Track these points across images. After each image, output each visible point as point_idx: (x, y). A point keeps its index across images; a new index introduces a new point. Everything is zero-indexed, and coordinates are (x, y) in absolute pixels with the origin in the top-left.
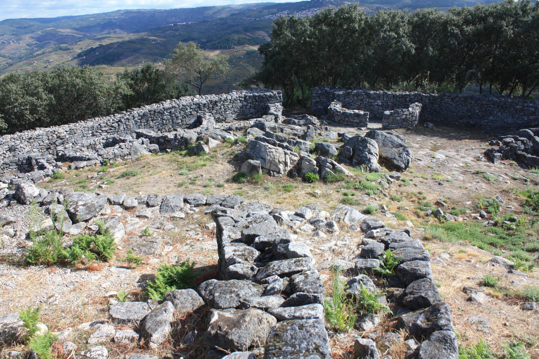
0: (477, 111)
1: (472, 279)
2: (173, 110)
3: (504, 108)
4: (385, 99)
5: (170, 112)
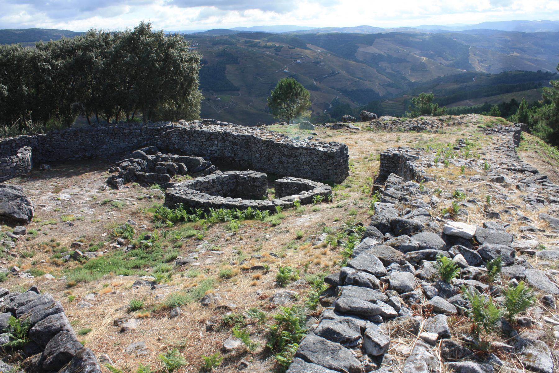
0: (90, 142)
1: (120, 309)
3: (114, 134)
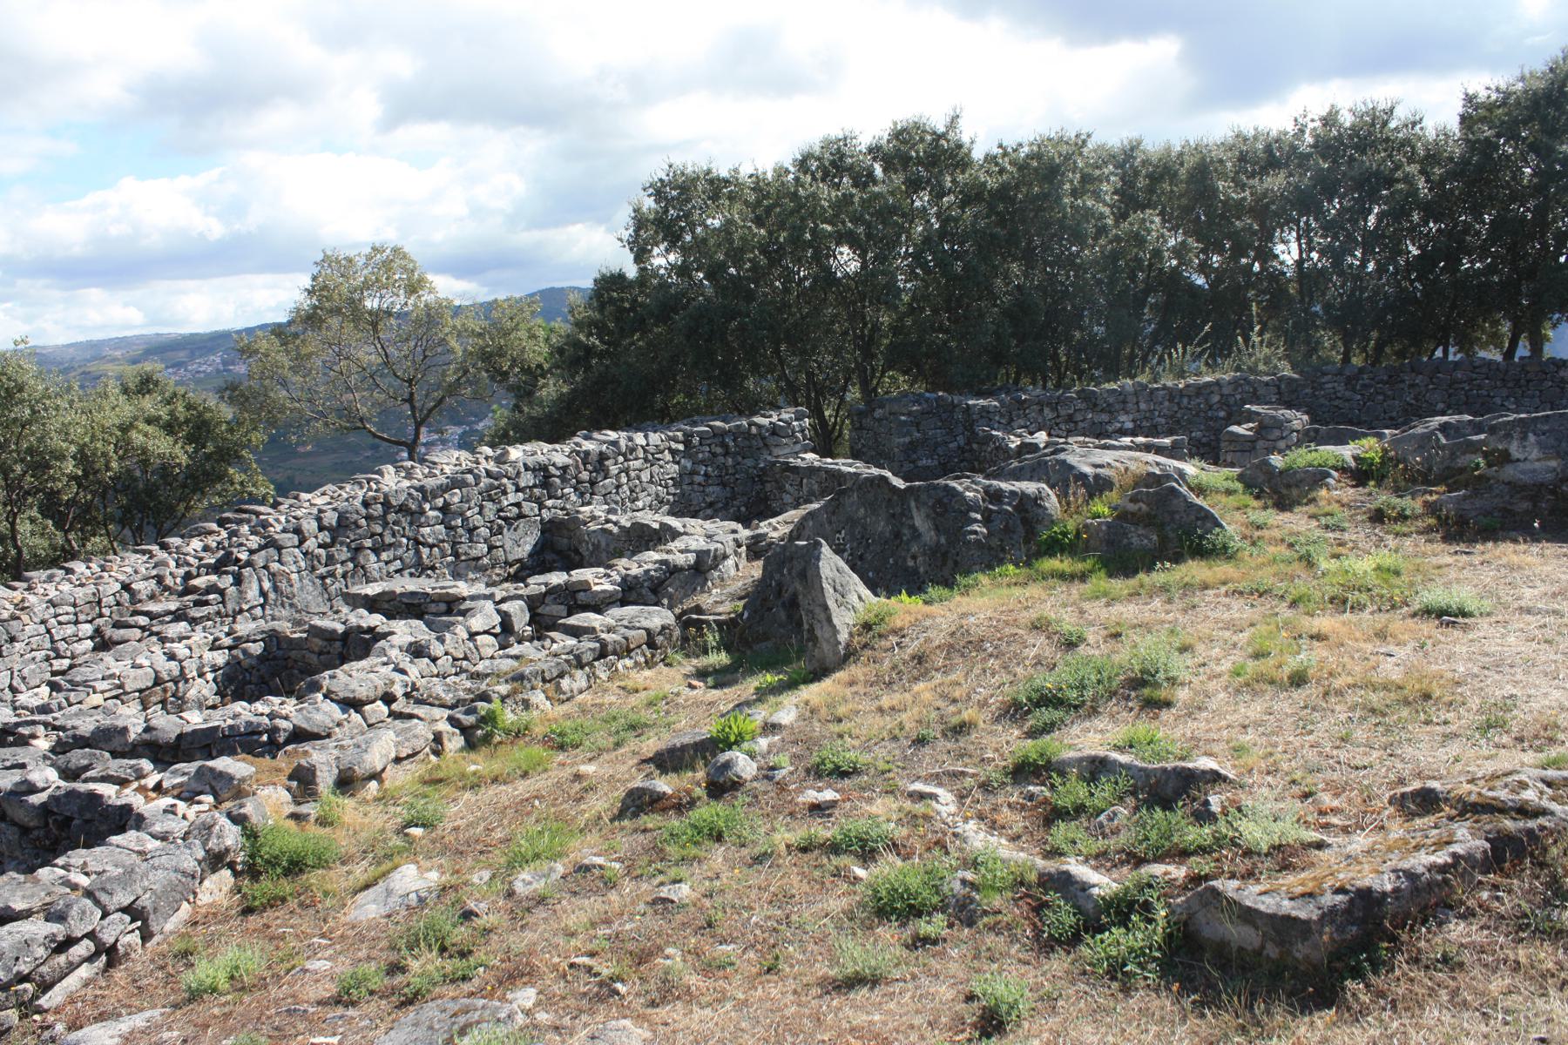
2: (455, 497)
4: (1143, 406)
5: (445, 509)
